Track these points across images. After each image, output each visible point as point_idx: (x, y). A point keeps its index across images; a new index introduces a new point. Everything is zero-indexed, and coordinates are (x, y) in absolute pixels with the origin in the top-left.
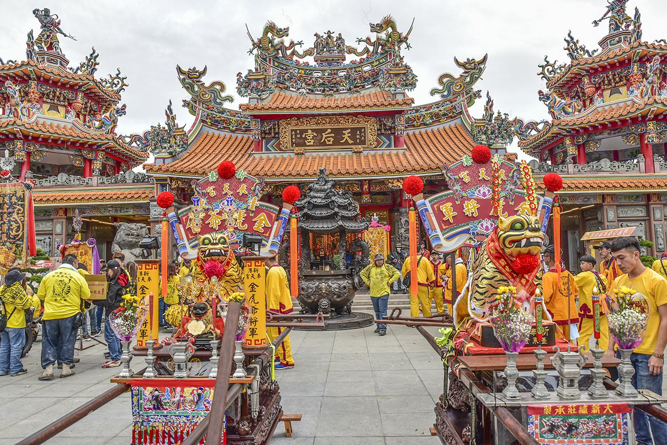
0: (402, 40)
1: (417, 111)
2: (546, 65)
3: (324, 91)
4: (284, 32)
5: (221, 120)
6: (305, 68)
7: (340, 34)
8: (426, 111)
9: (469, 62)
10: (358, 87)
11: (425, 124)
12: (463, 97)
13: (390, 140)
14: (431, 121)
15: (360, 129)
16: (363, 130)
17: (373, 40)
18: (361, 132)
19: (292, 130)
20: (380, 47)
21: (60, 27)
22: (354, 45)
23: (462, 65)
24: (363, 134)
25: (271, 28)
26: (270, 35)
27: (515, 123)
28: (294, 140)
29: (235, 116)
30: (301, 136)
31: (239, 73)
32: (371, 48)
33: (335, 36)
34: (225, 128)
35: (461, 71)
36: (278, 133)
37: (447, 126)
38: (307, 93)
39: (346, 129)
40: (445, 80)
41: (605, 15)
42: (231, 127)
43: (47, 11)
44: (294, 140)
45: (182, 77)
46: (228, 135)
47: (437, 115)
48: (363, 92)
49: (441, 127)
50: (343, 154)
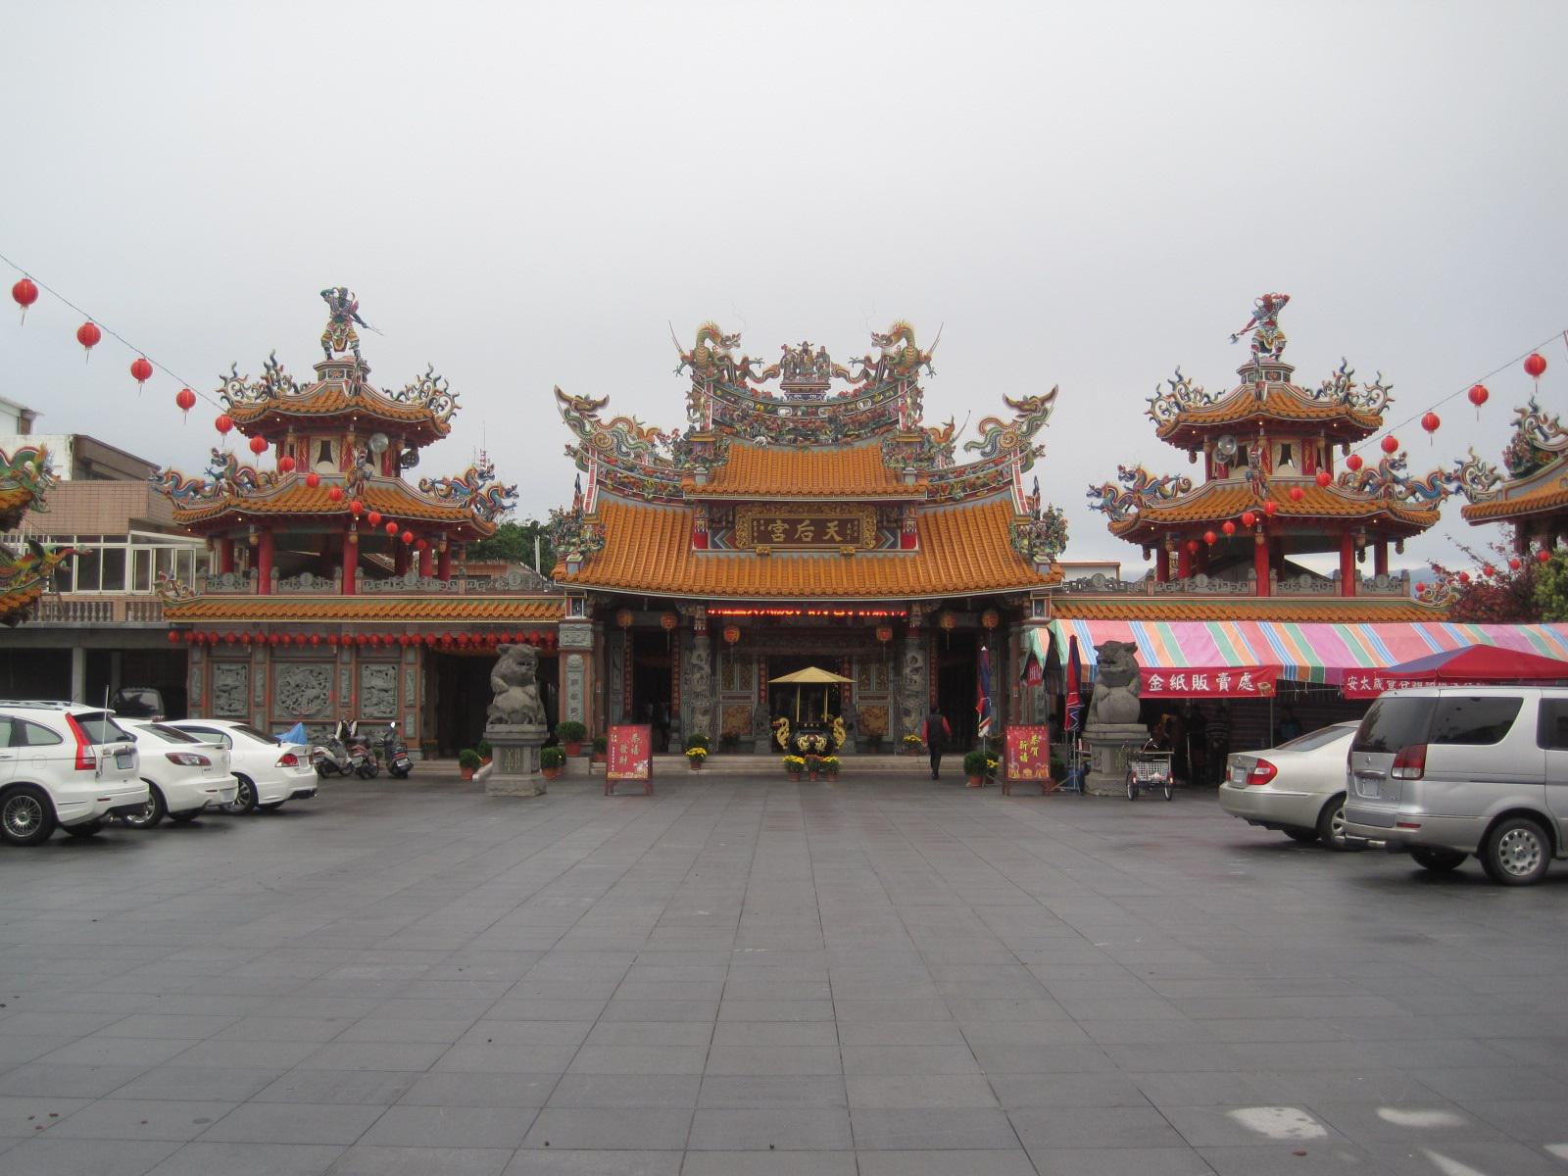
0: (922, 360)
1: (941, 477)
2: (1158, 399)
3: (795, 440)
4: (733, 340)
5: (629, 483)
6: (764, 401)
7: (823, 348)
8: (956, 477)
9: (1026, 402)
10: (850, 436)
11: (953, 499)
12: (1015, 455)
13: (896, 537)
14: (962, 494)
15: (852, 521)
16: (856, 523)
17: (875, 359)
18: (853, 526)
19: (753, 520)
20: (887, 371)
21: (358, 312)
22: (845, 364)
23: (1018, 406)
24: (856, 528)
25: (710, 332)
26: (709, 343)
27: (1105, 491)
28: (755, 534)
29: (651, 476)
30: (766, 528)
31: (676, 430)
32: (873, 373)
33: (815, 350)
34: (635, 495)
35: (1015, 412)
36: (733, 522)
37: (988, 501)
38: (769, 443)
39: (832, 520)
40: (988, 427)
41: (1250, 325)
42: (646, 495)
43: (344, 292)
44: (755, 534)
45: (564, 406)
46: (640, 505)
47: (973, 486)
48: (857, 444)
49: (979, 503)
50: (826, 556)
